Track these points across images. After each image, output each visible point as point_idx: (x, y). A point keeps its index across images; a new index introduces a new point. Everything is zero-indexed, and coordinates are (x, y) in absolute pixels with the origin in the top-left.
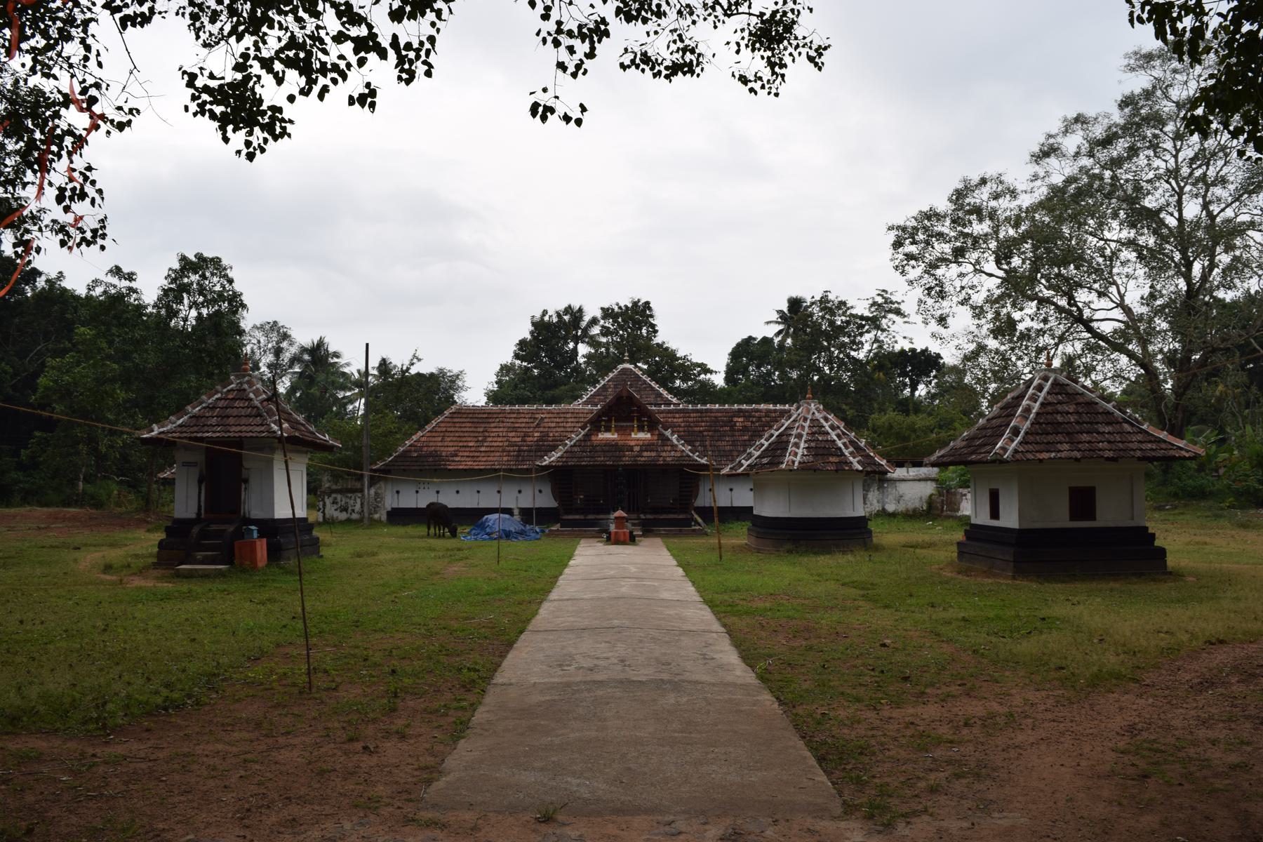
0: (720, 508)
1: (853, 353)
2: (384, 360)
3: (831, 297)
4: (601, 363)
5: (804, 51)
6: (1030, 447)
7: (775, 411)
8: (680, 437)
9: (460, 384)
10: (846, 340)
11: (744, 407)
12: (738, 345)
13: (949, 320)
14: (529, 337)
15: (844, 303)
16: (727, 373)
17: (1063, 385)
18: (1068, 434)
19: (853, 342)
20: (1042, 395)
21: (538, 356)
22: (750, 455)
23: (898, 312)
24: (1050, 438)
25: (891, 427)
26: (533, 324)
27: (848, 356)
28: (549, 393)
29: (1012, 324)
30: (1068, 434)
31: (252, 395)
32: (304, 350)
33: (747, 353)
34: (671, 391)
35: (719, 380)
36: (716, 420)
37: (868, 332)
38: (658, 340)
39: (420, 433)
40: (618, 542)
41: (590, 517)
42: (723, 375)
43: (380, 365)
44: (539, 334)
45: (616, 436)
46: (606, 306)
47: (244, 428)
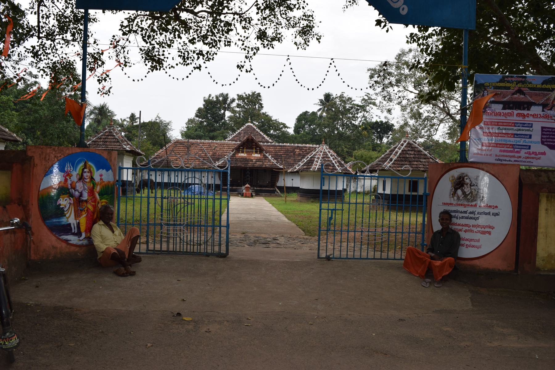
0: (287, 187)
1: (353, 122)
2: (132, 114)
3: (345, 95)
4: (238, 122)
5: (316, 36)
6: (395, 165)
7: (313, 147)
8: (272, 157)
9: (169, 127)
10: (351, 116)
11: (300, 145)
12: (301, 115)
13: (392, 111)
14: (202, 107)
15: (351, 99)
16: (295, 128)
17: (411, 144)
18: (410, 161)
19: (354, 117)
20: (403, 147)
21: (206, 115)
22: (299, 165)
23: (374, 104)
24: (403, 163)
25: (362, 157)
26: (205, 101)
27: (351, 123)
28: (212, 134)
29: (420, 114)
30: (410, 161)
31: (115, 134)
32: (95, 108)
33: (304, 119)
34: (268, 135)
35: (291, 131)
36: (288, 150)
37: (361, 112)
38: (263, 111)
39: (161, 150)
40: (246, 197)
41: (234, 188)
42: (293, 129)
43: (131, 116)
44: (208, 106)
45: (246, 155)
46: (240, 94)
47: (113, 146)
